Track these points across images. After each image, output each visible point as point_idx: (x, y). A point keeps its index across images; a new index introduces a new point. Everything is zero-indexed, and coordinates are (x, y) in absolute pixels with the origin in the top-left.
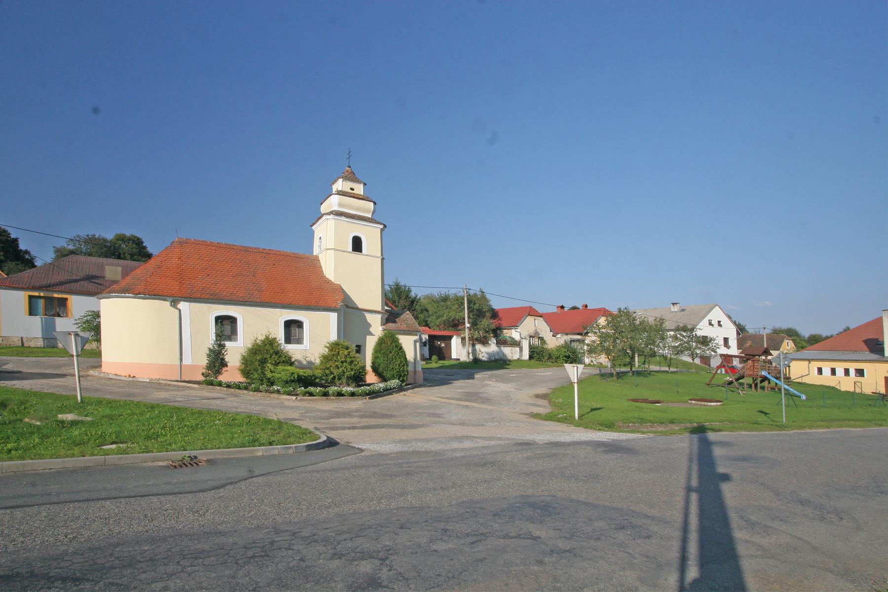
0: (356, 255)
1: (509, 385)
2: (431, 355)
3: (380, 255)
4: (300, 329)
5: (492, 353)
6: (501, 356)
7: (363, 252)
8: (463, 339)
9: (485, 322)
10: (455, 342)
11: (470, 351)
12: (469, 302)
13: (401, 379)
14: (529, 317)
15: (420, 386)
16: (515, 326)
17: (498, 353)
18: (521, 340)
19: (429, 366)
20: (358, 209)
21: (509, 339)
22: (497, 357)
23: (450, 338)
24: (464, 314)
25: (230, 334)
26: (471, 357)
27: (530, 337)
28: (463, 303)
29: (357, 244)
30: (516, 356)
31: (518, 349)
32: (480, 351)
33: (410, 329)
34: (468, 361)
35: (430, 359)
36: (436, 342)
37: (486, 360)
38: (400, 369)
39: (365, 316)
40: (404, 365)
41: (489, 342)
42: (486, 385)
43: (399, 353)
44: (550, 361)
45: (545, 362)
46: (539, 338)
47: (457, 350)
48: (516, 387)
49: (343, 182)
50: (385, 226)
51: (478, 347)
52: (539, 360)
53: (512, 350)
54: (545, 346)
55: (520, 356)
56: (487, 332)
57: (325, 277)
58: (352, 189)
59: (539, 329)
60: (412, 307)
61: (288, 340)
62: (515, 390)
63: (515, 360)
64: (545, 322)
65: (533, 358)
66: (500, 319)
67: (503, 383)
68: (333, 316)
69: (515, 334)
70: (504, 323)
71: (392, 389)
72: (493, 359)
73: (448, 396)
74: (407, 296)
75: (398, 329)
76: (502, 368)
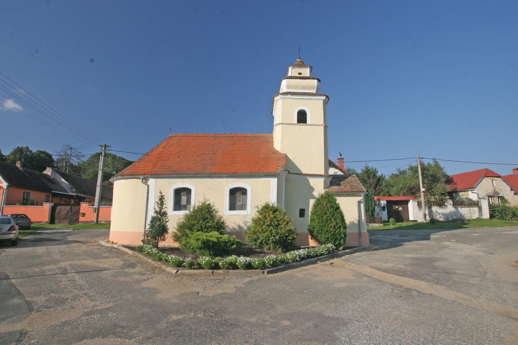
0: (302, 127)
1: (474, 247)
2: (389, 217)
3: (322, 122)
4: (244, 196)
5: (449, 214)
6: (459, 216)
7: (307, 123)
8: (419, 204)
9: (440, 187)
10: (412, 205)
11: (427, 213)
12: (423, 169)
13: (337, 243)
14: (486, 179)
15: (365, 249)
16: (472, 187)
17: (455, 214)
18: (480, 200)
19: (386, 228)
20: (304, 88)
21: (466, 200)
22: (455, 218)
23: (407, 202)
24: (419, 180)
25: (185, 204)
26: (428, 218)
27: (489, 196)
28: (417, 171)
29: (302, 117)
30: (476, 216)
31: (476, 209)
32: (437, 212)
33: (354, 190)
34: (425, 222)
35: (388, 221)
36: (393, 206)
37: (443, 220)
38: (335, 232)
39: (308, 180)
40: (340, 227)
41: (446, 204)
42: (445, 247)
43: (334, 214)
44: (514, 219)
45: (509, 220)
46: (499, 197)
47: (413, 213)
48: (484, 249)
49: (292, 69)
50: (327, 97)
51: (435, 209)
52: (502, 218)
53: (470, 210)
54: (507, 205)
55: (480, 215)
56: (442, 194)
57: (274, 149)
58: (300, 74)
59: (498, 188)
60: (378, 183)
61: (232, 207)
62: (485, 254)
63: (475, 219)
64: (504, 181)
65: (494, 217)
66: (455, 184)
67: (465, 244)
68: (274, 181)
69: (472, 196)
70: (459, 187)
71: (319, 256)
72: (451, 219)
73: (389, 265)
74: (374, 176)
75: (340, 191)
76: (461, 227)
